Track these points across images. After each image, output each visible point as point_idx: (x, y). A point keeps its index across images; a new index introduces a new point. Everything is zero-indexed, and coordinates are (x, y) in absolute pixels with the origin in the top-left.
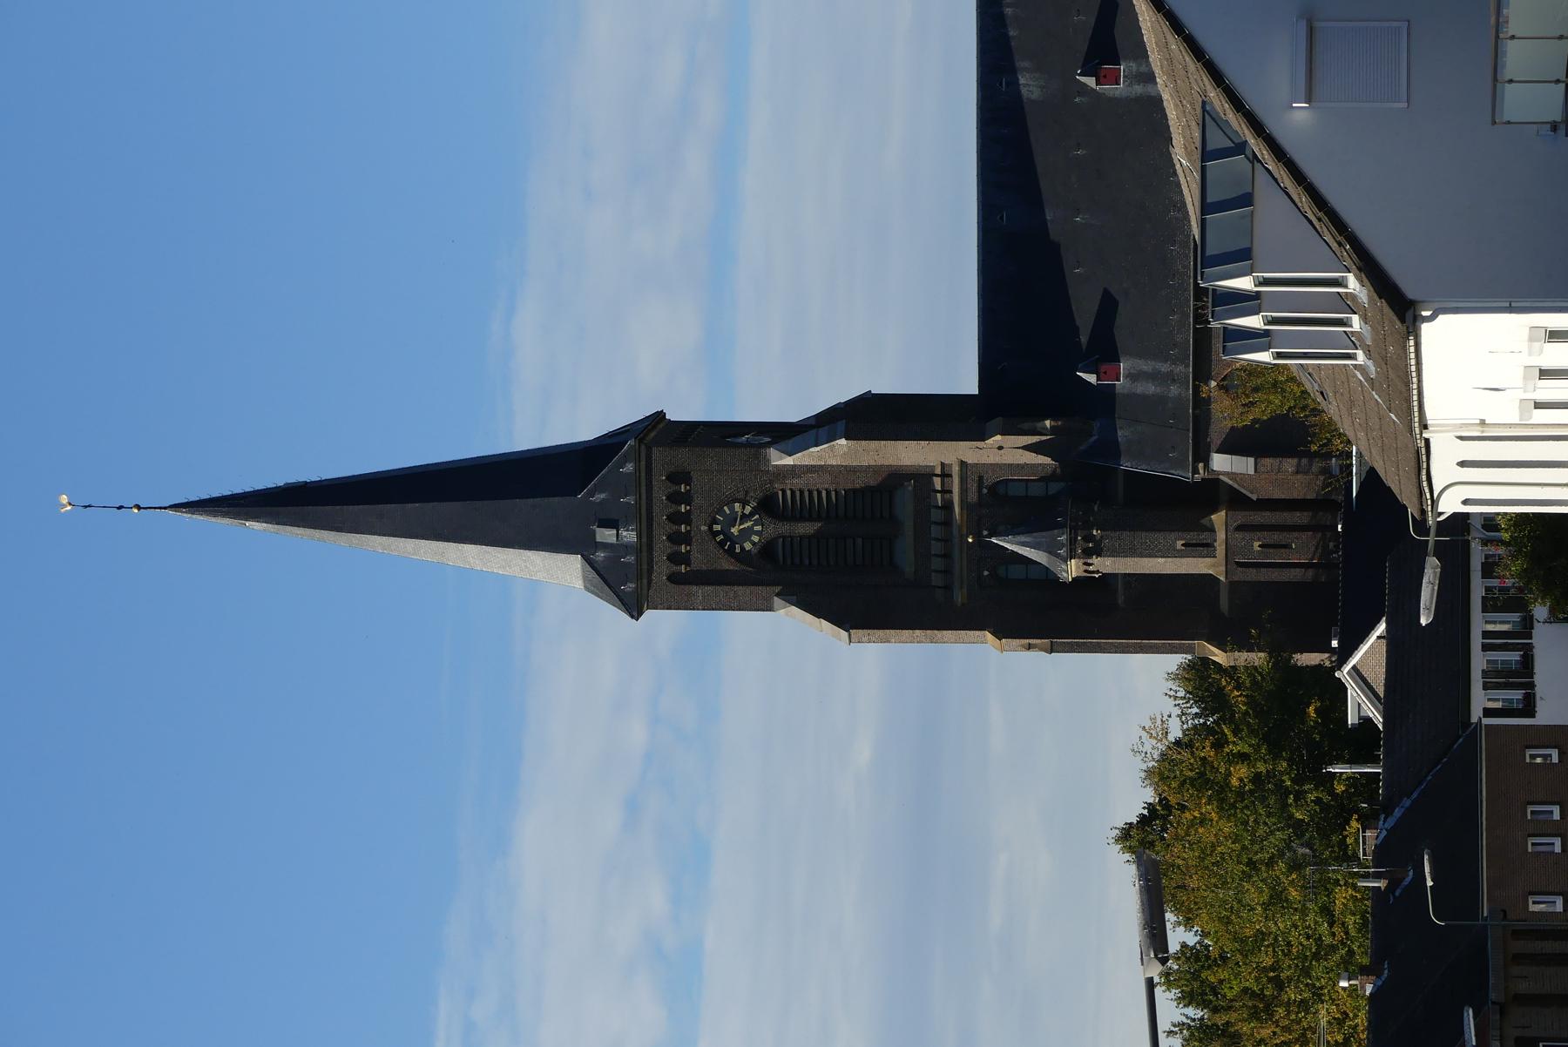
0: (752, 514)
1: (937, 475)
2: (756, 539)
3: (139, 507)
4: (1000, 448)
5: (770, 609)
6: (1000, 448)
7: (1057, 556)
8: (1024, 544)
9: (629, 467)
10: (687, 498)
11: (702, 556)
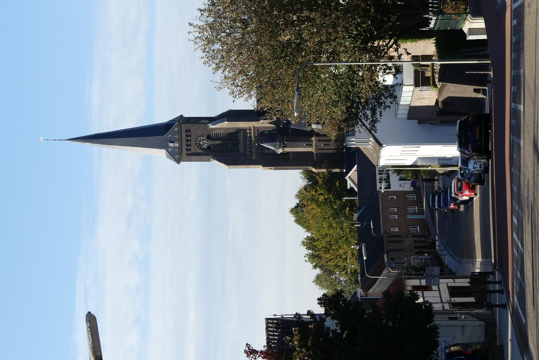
0: (205, 139)
1: (248, 130)
2: (206, 145)
3: (60, 140)
4: (263, 123)
5: (210, 161)
6: (263, 123)
7: (277, 148)
8: (269, 145)
9: (176, 129)
10: (190, 136)
11: (194, 149)
